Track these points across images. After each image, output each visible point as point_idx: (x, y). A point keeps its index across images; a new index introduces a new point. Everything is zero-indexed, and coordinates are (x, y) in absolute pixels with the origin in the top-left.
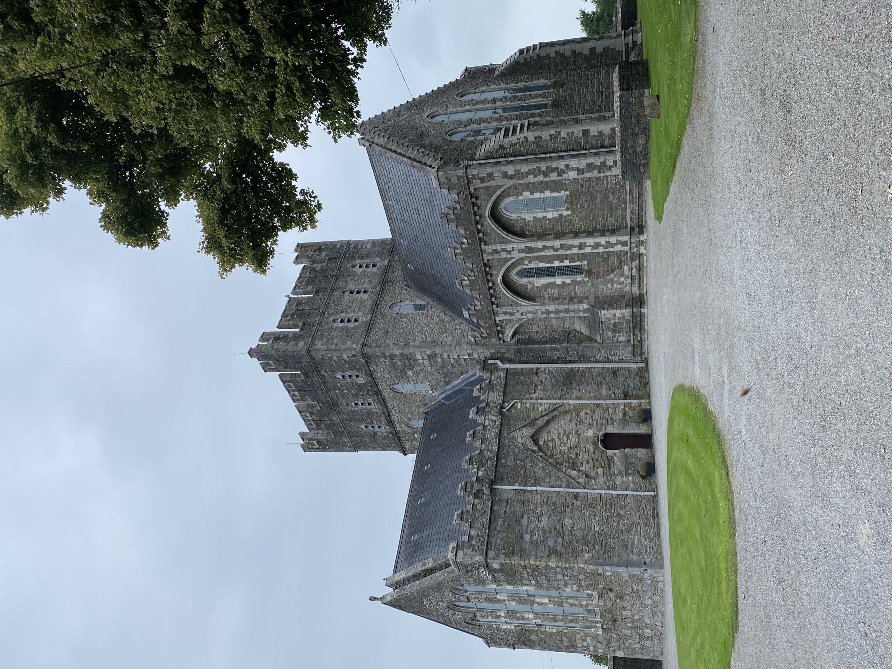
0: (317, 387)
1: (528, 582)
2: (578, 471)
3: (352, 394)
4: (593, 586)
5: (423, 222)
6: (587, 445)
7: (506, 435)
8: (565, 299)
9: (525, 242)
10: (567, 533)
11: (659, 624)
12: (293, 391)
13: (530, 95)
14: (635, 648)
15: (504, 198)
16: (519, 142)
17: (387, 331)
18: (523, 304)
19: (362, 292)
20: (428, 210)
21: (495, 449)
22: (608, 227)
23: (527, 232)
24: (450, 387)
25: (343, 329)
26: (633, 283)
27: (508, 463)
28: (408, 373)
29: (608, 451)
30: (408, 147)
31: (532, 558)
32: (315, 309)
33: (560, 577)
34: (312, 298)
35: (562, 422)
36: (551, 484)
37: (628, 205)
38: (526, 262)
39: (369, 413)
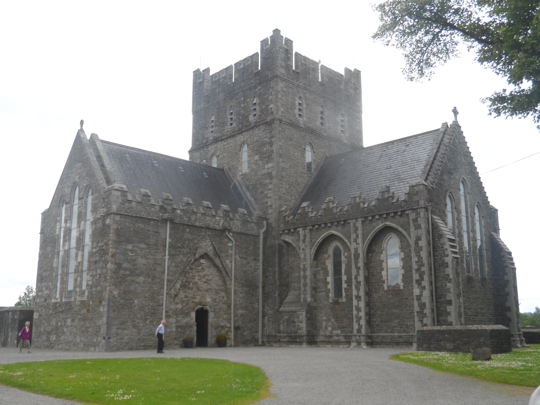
0: (246, 83)
1: (95, 246)
2: (180, 289)
3: (240, 110)
4: (91, 296)
5: (380, 172)
6: (199, 297)
7: (208, 233)
8: (315, 284)
9: (363, 253)
10: (133, 278)
11: (60, 346)
12: (244, 64)
13: (477, 260)
14: (41, 327)
16: (444, 250)
18: (312, 250)
19: (321, 121)
20: (390, 176)
21: (197, 224)
22: (372, 318)
25: (294, 104)
26: (326, 336)
27: (186, 234)
30: (442, 162)
31: (114, 250)
33: (99, 271)
34: (318, 81)
35: (217, 278)
36: (170, 268)
37: (389, 334)
38: (346, 254)
39: (224, 124)
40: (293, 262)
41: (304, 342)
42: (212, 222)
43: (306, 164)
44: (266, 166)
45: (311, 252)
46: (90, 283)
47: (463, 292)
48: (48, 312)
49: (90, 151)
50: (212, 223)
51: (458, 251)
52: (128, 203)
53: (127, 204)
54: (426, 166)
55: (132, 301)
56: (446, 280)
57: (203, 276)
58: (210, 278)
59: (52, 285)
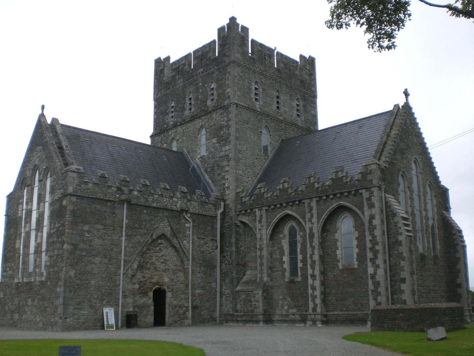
4: (48, 278)
6: (156, 277)
7: (165, 214)
9: (318, 232)
10: (90, 259)
15: (354, 217)
17: (248, 124)
18: (268, 230)
19: (277, 105)
21: (154, 205)
22: (328, 297)
23: (325, 234)
24: (202, 171)
25: (250, 89)
26: (282, 315)
28: (214, 139)
29: (152, 293)
31: (70, 231)
32: (265, 68)
33: (56, 252)
35: (175, 259)
38: (301, 234)
39: (183, 109)
40: (250, 242)
41: (261, 321)
42: (170, 203)
43: (262, 147)
44: (223, 149)
45: (267, 232)
46: (48, 263)
47: (417, 270)
48: (12, 291)
49: (48, 135)
50: (169, 204)
51: (411, 229)
52: (85, 185)
53: (83, 185)
54: (379, 146)
55: (88, 281)
56: (400, 258)
57: (160, 256)
58: (168, 258)
59: (15, 265)
